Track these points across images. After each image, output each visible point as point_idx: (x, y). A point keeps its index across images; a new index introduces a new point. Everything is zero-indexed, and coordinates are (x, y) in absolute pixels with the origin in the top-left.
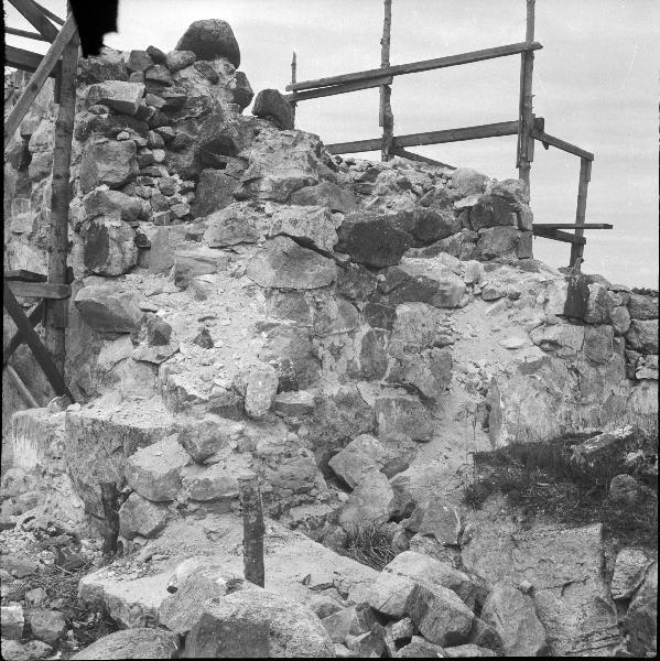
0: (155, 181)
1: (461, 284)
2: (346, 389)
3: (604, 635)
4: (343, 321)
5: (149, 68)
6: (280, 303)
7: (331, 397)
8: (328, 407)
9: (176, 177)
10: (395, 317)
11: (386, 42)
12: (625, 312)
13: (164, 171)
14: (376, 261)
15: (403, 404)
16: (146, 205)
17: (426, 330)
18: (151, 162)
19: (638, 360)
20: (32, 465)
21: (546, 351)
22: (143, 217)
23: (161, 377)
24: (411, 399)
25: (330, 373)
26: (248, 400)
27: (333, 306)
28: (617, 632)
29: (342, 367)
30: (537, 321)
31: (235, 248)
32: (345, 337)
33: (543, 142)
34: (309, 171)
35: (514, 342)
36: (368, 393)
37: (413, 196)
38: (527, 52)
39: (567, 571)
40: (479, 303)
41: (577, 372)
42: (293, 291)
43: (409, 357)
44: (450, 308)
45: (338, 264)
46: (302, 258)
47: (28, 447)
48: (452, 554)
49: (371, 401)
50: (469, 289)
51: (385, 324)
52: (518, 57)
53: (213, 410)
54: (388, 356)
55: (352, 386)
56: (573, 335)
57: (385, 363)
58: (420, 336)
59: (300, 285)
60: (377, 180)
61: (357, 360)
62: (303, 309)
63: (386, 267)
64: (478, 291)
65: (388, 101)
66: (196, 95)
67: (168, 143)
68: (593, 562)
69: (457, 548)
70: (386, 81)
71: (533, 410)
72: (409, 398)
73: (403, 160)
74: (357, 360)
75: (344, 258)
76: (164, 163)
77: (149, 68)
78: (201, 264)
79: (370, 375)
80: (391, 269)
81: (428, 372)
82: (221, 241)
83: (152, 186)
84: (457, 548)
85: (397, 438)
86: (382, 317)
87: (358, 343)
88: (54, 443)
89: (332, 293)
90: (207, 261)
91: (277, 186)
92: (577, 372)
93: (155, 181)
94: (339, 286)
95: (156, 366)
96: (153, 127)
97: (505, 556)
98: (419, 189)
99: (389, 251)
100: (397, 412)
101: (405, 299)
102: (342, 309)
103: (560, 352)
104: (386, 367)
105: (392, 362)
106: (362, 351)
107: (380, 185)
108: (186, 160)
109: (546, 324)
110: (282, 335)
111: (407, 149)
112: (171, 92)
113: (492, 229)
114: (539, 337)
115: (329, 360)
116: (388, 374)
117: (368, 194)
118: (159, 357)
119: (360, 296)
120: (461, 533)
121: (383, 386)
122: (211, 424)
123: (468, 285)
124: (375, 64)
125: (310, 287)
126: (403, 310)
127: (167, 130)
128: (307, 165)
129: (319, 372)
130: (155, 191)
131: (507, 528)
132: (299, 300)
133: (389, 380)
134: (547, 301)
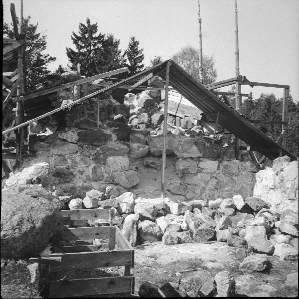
2: (85, 184)
14: (96, 143)
29: (84, 177)
33: (251, 86)
43: (115, 174)
54: (104, 173)
57: (103, 176)
75: (79, 144)
81: (124, 179)
86: (100, 161)
102: (82, 159)
103: (204, 171)
106: (92, 172)
115: (78, 175)
116: (104, 179)
119: (90, 154)
121: (103, 183)
126: (110, 159)
129: (74, 179)
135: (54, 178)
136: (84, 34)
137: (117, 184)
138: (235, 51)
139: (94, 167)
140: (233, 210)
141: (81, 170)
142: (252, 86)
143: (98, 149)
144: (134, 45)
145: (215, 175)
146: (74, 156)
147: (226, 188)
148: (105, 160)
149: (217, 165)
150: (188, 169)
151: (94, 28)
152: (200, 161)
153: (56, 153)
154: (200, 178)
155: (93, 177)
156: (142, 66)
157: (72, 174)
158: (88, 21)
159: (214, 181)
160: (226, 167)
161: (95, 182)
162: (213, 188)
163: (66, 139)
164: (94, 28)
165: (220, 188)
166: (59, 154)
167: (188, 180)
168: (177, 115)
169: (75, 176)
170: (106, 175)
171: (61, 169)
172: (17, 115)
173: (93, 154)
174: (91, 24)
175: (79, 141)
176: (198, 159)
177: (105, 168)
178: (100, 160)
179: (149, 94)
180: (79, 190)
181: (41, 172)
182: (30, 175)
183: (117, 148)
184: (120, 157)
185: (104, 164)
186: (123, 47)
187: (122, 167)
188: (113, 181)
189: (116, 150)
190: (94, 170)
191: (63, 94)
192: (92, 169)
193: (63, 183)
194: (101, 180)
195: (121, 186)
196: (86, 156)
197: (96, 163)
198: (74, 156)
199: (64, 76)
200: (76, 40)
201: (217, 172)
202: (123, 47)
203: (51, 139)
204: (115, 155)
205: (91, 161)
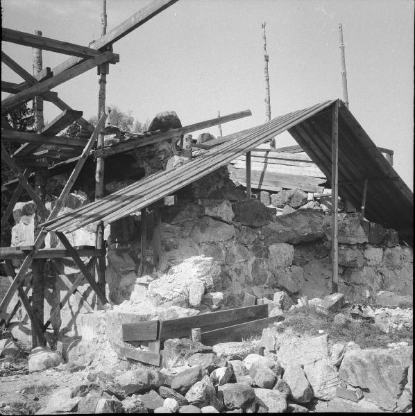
3: (332, 381)
4: (240, 256)
6: (207, 250)
8: (236, 301)
10: (269, 251)
14: (255, 224)
20: (91, 338)
23: (149, 290)
25: (236, 283)
26: (190, 298)
28: (337, 380)
29: (242, 278)
32: (243, 264)
39: (315, 355)
41: (381, 274)
42: (213, 243)
43: (278, 272)
45: (235, 227)
47: (89, 330)
48: (273, 354)
53: (175, 304)
54: (267, 272)
61: (250, 275)
62: (219, 251)
65: (101, 89)
68: (324, 350)
69: (275, 352)
74: (250, 275)
81: (290, 279)
84: (275, 352)
88: (101, 327)
89: (234, 242)
92: (381, 274)
94: (237, 238)
95: (146, 285)
97: (293, 352)
99: (262, 218)
101: (274, 242)
102: (239, 250)
105: (269, 275)
106: (253, 270)
118: (148, 281)
119: (249, 242)
120: (275, 345)
121: (265, 288)
122: (172, 311)
131: (294, 339)
138: (265, 96)
150: (355, 261)
152: (365, 248)
153: (206, 240)
154: (365, 274)
167: (354, 278)
168: (262, 188)
172: (97, 180)
173: (253, 240)
176: (363, 246)
177: (267, 262)
181: (211, 270)
182: (199, 277)
183: (281, 231)
185: (266, 256)
189: (280, 234)
191: (165, 146)
192: (252, 265)
194: (264, 283)
197: (257, 256)
203: (183, 218)
204: (277, 242)
205: (249, 253)
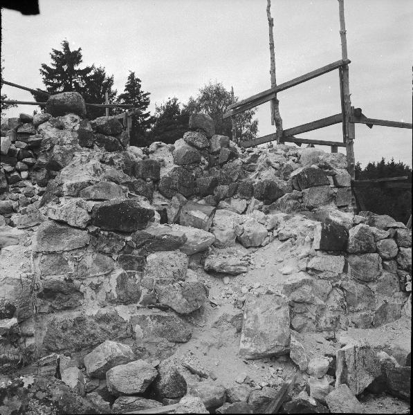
0: (21, 190)
1: (263, 230)
2: (104, 311)
5: (18, 127)
6: (44, 260)
7: (92, 317)
9: (36, 186)
11: (273, 71)
12: (392, 242)
13: (28, 184)
15: (159, 318)
16: (14, 204)
17: (175, 269)
18: (18, 179)
19: (406, 278)
21: (311, 275)
22: (14, 210)
24: (166, 315)
27: (89, 259)
29: (101, 296)
30: (303, 254)
31: (33, 228)
33: (368, 125)
34: (94, 176)
35: (287, 269)
36: (125, 313)
37: (273, 170)
38: (343, 67)
40: (276, 242)
42: (54, 253)
43: (162, 287)
44: (256, 247)
46: (61, 231)
49: (126, 318)
50: (270, 234)
51: (136, 268)
52: (337, 70)
55: (110, 308)
56: (334, 263)
57: (139, 293)
58: (171, 273)
59: (57, 249)
60: (258, 161)
61: (114, 292)
63: (134, 231)
64: (275, 234)
65: (277, 109)
66: (46, 137)
67: (30, 167)
70: (272, 97)
71: (269, 320)
72: (164, 314)
73: (293, 144)
74: (114, 292)
75: (92, 229)
76: (28, 178)
77: (18, 127)
78: (11, 239)
79: (127, 300)
80: (138, 232)
81: (179, 297)
82: (24, 225)
83: (20, 193)
85: (155, 341)
86: (133, 263)
87: (114, 282)
90: (13, 238)
91: (69, 187)
92: (342, 288)
93: (21, 190)
96: (20, 160)
98: (277, 165)
100: (152, 325)
101: (153, 249)
102: (96, 261)
103: (321, 275)
104: (140, 296)
107: (260, 164)
108: (41, 176)
109: (309, 256)
110: (8, 284)
111: (297, 136)
112: (32, 138)
113: (308, 189)
114: (304, 266)
115: (89, 293)
116: (141, 299)
117: (253, 171)
119: (113, 251)
121: (138, 308)
123: (269, 231)
124: (267, 86)
125: (67, 249)
126: (152, 257)
127: (29, 160)
128: (93, 173)
129: (81, 301)
130: (20, 195)
132: (59, 258)
133: (144, 303)
134: (312, 240)
135: (39, 301)
136: (59, 66)
137: (165, 308)
139: (121, 275)
140: (295, 326)
141: (95, 281)
142: (370, 126)
143: (129, 238)
144: (133, 84)
145: (339, 283)
146: (81, 254)
147: (360, 306)
148: (142, 260)
149: (343, 263)
151: (75, 57)
155: (119, 296)
156: (147, 115)
157: (77, 290)
158: (66, 46)
159: (338, 295)
160: (356, 267)
161: (122, 306)
162: (336, 306)
163: (64, 220)
164: (75, 57)
165: (349, 305)
166: (51, 250)
169: (82, 294)
170: (144, 292)
171: (54, 282)
173: (119, 248)
174: (72, 50)
175: (89, 224)
177: (141, 276)
178: (133, 262)
179: (191, 144)
180: (91, 323)
184: (171, 254)
185: (141, 269)
186: (119, 88)
187: (174, 273)
188: (158, 301)
190: (122, 282)
192: (117, 279)
193: (59, 311)
194: (135, 302)
195: (173, 310)
196: (104, 253)
198: (81, 254)
199: (54, 100)
200: (49, 74)
201: (343, 277)
202: (119, 88)
205: (115, 264)
